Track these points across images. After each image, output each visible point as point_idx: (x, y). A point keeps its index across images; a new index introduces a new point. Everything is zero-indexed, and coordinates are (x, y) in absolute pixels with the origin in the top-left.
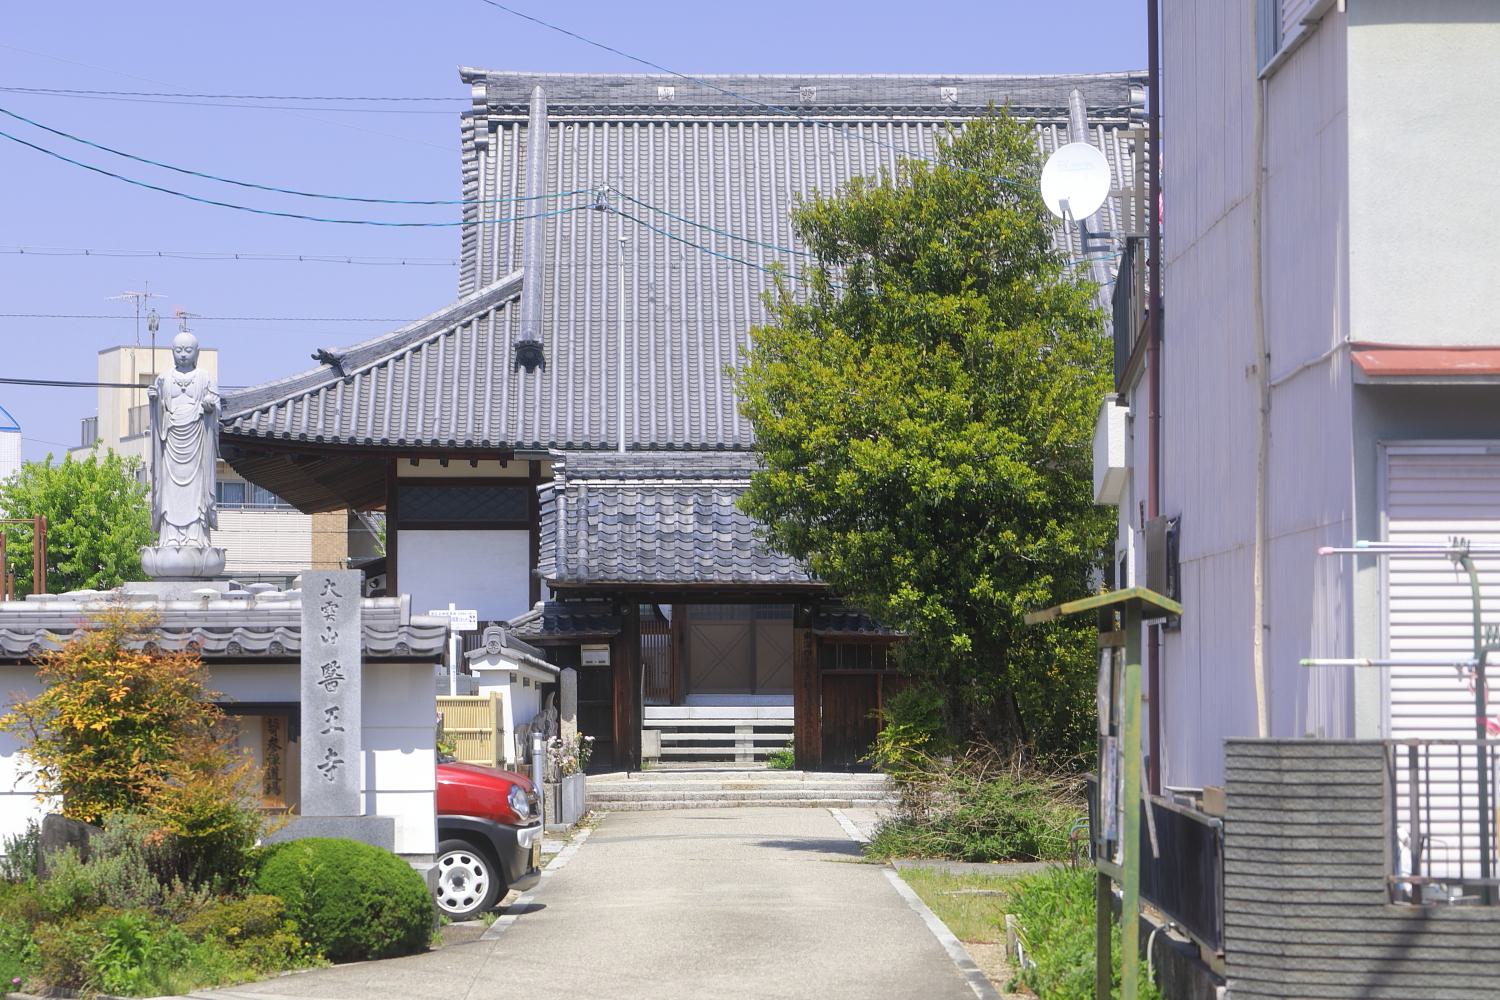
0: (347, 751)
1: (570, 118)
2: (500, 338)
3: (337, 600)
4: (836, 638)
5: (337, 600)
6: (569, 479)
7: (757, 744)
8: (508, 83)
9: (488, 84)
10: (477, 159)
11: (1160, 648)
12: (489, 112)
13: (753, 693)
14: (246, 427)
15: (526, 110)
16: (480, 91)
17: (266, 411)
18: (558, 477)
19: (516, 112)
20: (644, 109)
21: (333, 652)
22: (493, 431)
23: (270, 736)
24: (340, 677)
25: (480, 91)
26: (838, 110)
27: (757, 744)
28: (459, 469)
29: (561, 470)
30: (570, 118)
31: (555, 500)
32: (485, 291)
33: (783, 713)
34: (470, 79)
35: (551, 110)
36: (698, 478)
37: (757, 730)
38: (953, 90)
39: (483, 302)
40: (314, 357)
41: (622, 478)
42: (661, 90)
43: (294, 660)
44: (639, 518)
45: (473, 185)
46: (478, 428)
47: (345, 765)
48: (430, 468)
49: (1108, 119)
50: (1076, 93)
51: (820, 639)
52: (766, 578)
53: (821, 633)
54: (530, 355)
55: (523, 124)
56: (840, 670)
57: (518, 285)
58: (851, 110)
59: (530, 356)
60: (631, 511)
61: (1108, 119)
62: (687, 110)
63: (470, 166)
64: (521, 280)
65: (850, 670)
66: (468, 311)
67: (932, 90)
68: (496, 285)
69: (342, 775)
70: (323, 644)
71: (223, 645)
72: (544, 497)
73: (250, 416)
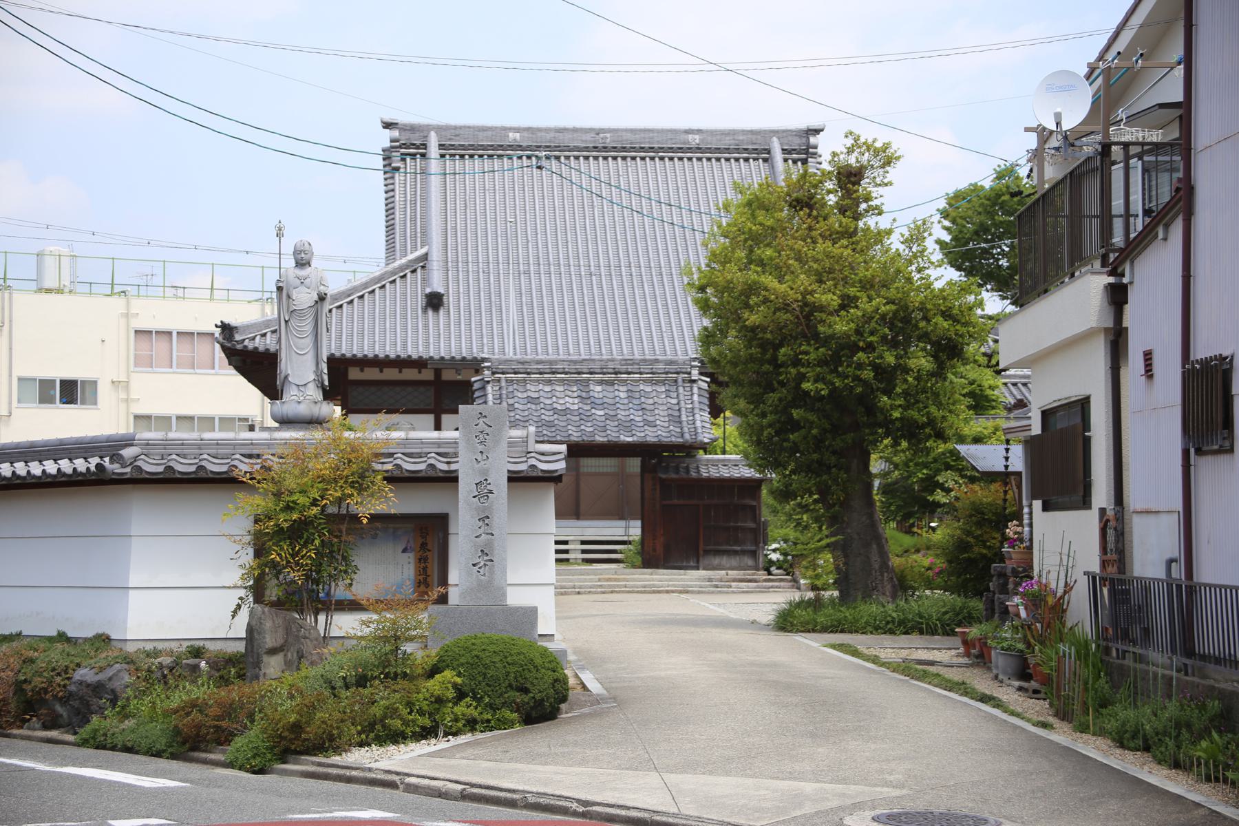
0: (496, 552)
1: (453, 152)
2: (414, 291)
3: (488, 430)
4: (672, 480)
5: (488, 430)
6: (493, 373)
7: (584, 552)
8: (412, 129)
9: (400, 129)
10: (393, 178)
11: (1192, 468)
12: (400, 147)
13: (578, 519)
14: (250, 345)
15: (425, 146)
16: (396, 133)
17: (264, 335)
18: (486, 372)
19: (418, 148)
20: (501, 147)
21: (485, 472)
22: (414, 350)
23: (420, 541)
24: (491, 492)
25: (396, 133)
26: (624, 149)
27: (584, 552)
28: (391, 374)
29: (488, 368)
30: (453, 152)
31: (483, 388)
32: (404, 261)
33: (635, 530)
34: (388, 125)
35: (441, 146)
36: (579, 373)
37: (583, 543)
38: (697, 137)
39: (402, 268)
40: (817, 131)
41: (528, 373)
42: (511, 135)
43: (451, 479)
44: (542, 400)
45: (391, 194)
46: (405, 347)
47: (496, 563)
48: (372, 374)
49: (795, 156)
50: (775, 139)
51: (662, 481)
52: (630, 439)
53: (664, 476)
54: (435, 301)
55: (423, 155)
56: (676, 501)
57: (425, 257)
58: (633, 149)
59: (434, 302)
60: (536, 395)
61: (795, 156)
62: (528, 148)
63: (389, 181)
64: (427, 254)
65: (681, 502)
66: (393, 273)
67: (684, 137)
68: (411, 257)
69: (492, 572)
70: (477, 466)
71: (422, 467)
72: (476, 386)
73: (253, 339)
